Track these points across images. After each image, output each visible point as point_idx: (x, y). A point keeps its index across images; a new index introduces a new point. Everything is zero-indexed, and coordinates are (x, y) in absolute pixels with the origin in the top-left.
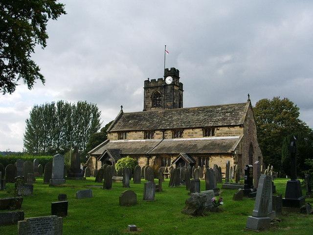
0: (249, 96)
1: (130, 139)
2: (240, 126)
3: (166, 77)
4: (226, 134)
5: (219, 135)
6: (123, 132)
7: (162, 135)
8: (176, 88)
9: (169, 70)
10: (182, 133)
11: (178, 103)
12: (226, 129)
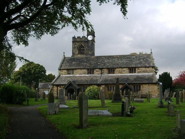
0: (64, 53)
1: (76, 74)
3: (88, 35)
4: (144, 72)
5: (139, 72)
7: (101, 72)
9: (81, 37)
10: (114, 71)
12: (144, 69)
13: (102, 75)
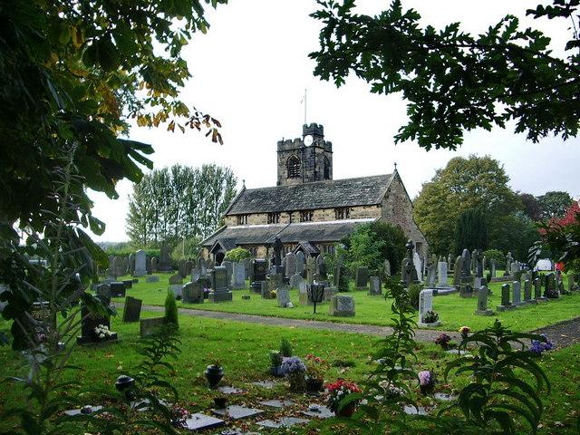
2: (378, 205)
3: (304, 136)
4: (362, 216)
6: (243, 215)
8: (317, 150)
11: (322, 171)
12: (361, 210)
13: (292, 224)
